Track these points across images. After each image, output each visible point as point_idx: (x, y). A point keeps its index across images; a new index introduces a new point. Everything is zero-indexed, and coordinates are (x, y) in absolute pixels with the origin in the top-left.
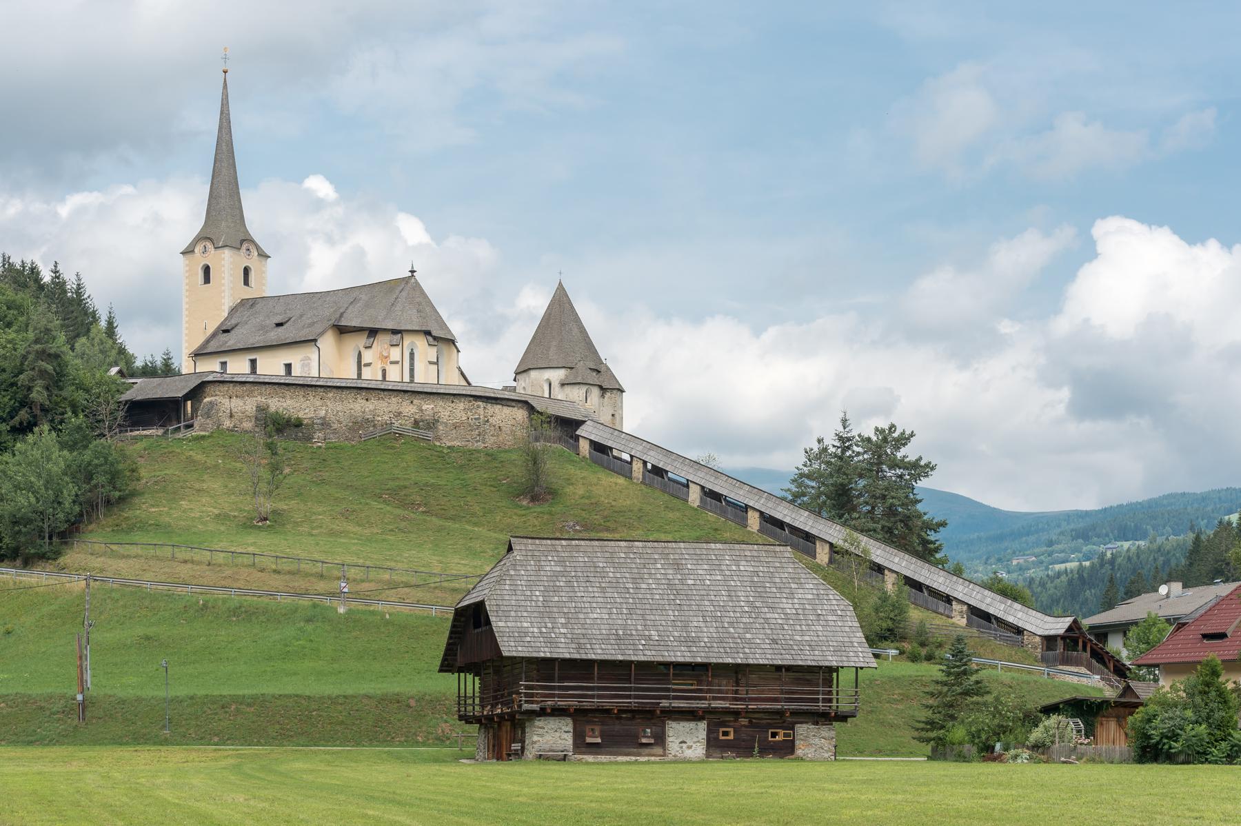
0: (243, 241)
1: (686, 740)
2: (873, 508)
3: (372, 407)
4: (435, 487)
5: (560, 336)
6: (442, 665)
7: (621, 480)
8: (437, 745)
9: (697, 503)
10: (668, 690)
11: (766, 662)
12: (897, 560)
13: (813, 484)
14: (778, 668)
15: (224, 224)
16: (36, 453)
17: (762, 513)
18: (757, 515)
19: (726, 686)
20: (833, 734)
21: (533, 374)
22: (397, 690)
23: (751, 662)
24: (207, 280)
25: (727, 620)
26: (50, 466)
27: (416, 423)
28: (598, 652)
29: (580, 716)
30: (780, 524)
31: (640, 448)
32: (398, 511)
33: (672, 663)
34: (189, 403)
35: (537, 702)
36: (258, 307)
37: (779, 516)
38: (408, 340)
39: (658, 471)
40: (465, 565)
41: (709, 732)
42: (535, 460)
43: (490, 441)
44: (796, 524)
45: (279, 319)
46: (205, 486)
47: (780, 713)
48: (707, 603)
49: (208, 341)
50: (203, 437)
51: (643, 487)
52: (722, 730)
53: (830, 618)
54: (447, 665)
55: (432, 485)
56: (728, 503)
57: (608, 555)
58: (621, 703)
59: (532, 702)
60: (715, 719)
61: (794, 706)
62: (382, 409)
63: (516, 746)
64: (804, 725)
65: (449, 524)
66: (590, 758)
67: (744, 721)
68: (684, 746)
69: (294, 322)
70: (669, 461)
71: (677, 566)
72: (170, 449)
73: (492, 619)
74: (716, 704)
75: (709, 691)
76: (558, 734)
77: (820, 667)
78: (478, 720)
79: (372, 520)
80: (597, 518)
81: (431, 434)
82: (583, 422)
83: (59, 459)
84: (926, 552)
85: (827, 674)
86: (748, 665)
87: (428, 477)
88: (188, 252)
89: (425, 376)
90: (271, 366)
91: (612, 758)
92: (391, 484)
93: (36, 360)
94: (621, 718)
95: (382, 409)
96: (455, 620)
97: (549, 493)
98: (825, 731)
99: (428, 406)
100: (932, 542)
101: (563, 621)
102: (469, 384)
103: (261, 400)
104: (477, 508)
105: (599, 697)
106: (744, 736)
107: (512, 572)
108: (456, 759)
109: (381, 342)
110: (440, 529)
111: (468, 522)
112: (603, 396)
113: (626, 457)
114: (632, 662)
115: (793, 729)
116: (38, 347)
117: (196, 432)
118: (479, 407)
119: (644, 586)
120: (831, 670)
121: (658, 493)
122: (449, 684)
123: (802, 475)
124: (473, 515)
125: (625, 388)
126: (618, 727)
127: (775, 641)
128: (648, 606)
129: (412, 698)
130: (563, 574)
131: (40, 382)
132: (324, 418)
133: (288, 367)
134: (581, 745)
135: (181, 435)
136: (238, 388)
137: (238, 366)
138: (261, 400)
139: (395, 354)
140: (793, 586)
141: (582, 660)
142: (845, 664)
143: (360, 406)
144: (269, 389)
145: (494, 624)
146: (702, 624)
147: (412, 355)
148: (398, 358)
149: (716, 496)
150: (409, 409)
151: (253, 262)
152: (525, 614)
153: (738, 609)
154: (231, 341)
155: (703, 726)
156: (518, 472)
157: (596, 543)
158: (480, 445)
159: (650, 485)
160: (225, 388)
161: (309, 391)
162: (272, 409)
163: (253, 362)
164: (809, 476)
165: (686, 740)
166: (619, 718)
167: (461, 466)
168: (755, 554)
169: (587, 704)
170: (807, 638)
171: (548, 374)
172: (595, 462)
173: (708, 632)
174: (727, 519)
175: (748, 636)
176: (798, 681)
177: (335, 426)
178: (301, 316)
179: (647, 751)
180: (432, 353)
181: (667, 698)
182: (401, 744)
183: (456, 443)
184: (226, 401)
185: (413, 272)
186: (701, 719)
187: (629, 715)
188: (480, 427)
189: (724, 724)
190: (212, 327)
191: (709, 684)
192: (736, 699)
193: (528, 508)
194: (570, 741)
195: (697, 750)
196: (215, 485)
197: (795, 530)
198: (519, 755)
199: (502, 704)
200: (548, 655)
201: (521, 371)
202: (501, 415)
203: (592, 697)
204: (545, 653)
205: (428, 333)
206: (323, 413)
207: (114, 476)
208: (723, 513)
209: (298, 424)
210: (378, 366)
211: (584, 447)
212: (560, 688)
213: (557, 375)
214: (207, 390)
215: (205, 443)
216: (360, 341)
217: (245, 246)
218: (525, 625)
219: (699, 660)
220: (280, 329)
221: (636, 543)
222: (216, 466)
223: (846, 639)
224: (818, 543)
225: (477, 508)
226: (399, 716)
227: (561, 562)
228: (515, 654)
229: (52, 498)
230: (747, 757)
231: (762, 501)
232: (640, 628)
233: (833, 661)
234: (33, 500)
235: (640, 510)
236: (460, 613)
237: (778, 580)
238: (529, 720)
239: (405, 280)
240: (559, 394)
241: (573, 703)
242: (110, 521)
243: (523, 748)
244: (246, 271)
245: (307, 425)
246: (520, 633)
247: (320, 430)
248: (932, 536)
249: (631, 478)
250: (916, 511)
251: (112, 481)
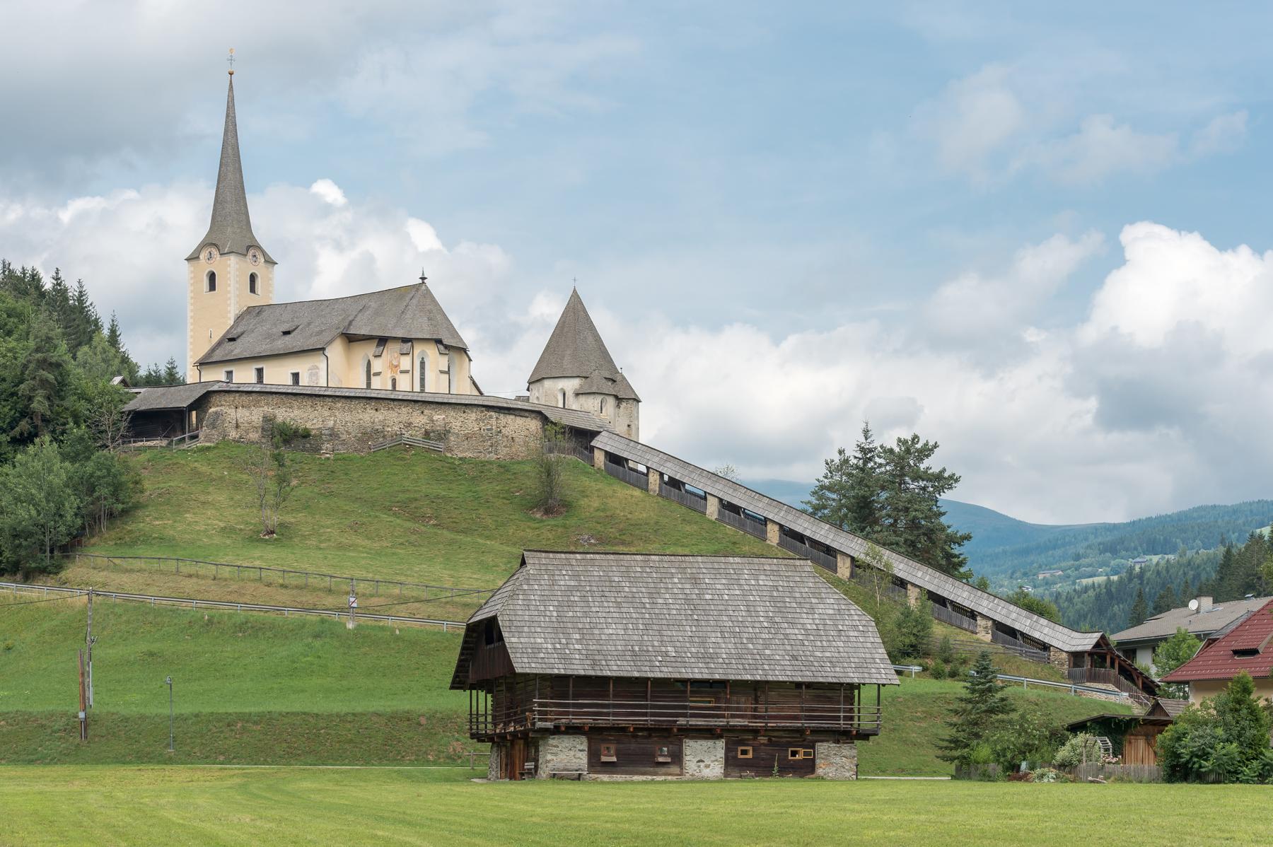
0: (250, 247)
1: (704, 759)
2: (896, 521)
3: (381, 418)
4: (447, 500)
5: (574, 344)
6: (453, 682)
7: (637, 493)
8: (448, 764)
9: (715, 516)
10: (685, 707)
11: (786, 679)
12: (920, 574)
13: (834, 496)
14: (798, 685)
15: (230, 230)
16: (37, 465)
17: (781, 526)
18: (776, 528)
19: (745, 703)
20: (854, 752)
21: (547, 383)
22: (407, 707)
23: (770, 678)
24: (212, 287)
25: (746, 635)
26: (51, 478)
27: (427, 433)
28: (614, 668)
29: (595, 734)
30: (800, 538)
31: (657, 459)
32: (409, 524)
33: (689, 680)
34: (194, 413)
35: (551, 720)
36: (265, 314)
37: (799, 529)
38: (418, 349)
39: (675, 483)
40: (477, 579)
41: (728, 750)
42: (548, 472)
43: (503, 452)
44: (817, 538)
45: (286, 327)
46: (210, 498)
47: (800, 731)
48: (725, 618)
49: (213, 350)
50: (208, 448)
51: (660, 499)
52: (740, 748)
53: (852, 634)
54: (459, 682)
55: (444, 497)
56: (747, 516)
57: (623, 569)
58: (637, 721)
59: (546, 720)
60: (734, 738)
61: (814, 724)
62: (392, 420)
63: (529, 765)
64: (825, 744)
65: (460, 537)
66: (605, 778)
67: (763, 740)
68: (702, 765)
69: (301, 330)
70: (686, 473)
71: (695, 581)
72: (175, 461)
73: (505, 635)
74: (735, 722)
75: (727, 709)
76: (572, 753)
77: (842, 684)
78: (490, 738)
79: (382, 533)
80: (612, 532)
81: (442, 445)
82: (598, 433)
83: (61, 471)
84: (950, 566)
85: (848, 691)
86: (767, 682)
87: (439, 490)
88: (193, 258)
89: (436, 385)
90: (278, 375)
91: (628, 777)
92: (401, 497)
93: (37, 369)
94: (637, 736)
95: (392, 420)
96: (466, 636)
97: (564, 506)
98: (846, 750)
99: (439, 416)
100: (956, 556)
101: (577, 636)
102: (481, 394)
103: (268, 410)
104: (489, 521)
105: (615, 714)
106: (763, 755)
107: (525, 587)
108: (468, 778)
109: (391, 351)
110: (451, 543)
111: (480, 535)
112: (618, 406)
113: (642, 469)
114: (648, 679)
115: (813, 748)
116: (39, 355)
117: (201, 443)
118: (491, 417)
119: (660, 601)
120: (852, 687)
121: (675, 506)
122: (461, 701)
123: (822, 487)
124: (486, 528)
125: (641, 398)
126: (634, 746)
127: (794, 658)
128: (664, 622)
129: (423, 715)
130: (577, 588)
131: (41, 392)
132: (332, 429)
133: (296, 376)
134: (596, 764)
135: (185, 446)
136: (244, 398)
137: (244, 376)
138: (268, 410)
139: (405, 363)
140: (814, 601)
141: (597, 677)
142: (867, 681)
143: (369, 417)
144: (276, 399)
145: (506, 640)
146: (720, 640)
147: (422, 364)
148: (408, 367)
149: (735, 509)
150: (420, 419)
151: (260, 269)
152: (539, 630)
153: (757, 625)
154: (237, 349)
155: (721, 744)
156: (532, 484)
157: (612, 557)
158: (493, 457)
159: (667, 498)
160: (230, 398)
161: (317, 401)
162: (280, 420)
163: (260, 371)
164: (829, 489)
165: (704, 759)
166: (635, 736)
167: (473, 478)
168: (775, 568)
169: (602, 722)
170: (828, 654)
171: (562, 384)
172: (611, 474)
173: (726, 649)
174: (746, 532)
175: (767, 652)
176: (818, 699)
177: (344, 437)
178: (309, 324)
179: (664, 770)
180: (443, 362)
181: (685, 715)
182: (412, 763)
183: (468, 455)
184: (232, 411)
185: (423, 279)
186: (719, 737)
187: (645, 733)
188: (492, 438)
189: (742, 742)
190: (218, 335)
191: (728, 701)
192: (755, 717)
193: (542, 521)
194: (585, 760)
195: (715, 769)
196: (221, 497)
197: (815, 544)
198: (533, 774)
199: (515, 722)
200: (563, 672)
201: (534, 381)
202: (514, 425)
203: (608, 714)
204: (559, 669)
205: (439, 341)
206: (331, 424)
207: (117, 488)
208: (742, 526)
209: (306, 435)
210: (388, 376)
211: (599, 458)
212: (575, 705)
213: (571, 385)
214: (213, 400)
215: (210, 455)
216: (370, 349)
217: (251, 252)
218: (539, 640)
219: (717, 677)
220: (288, 337)
221: (653, 557)
222: (222, 478)
223: (868, 656)
224: (839, 557)
225: (489, 521)
226: (410, 735)
227: (576, 576)
228: (528, 671)
229: (53, 510)
230: (767, 776)
231: (782, 514)
232: (656, 644)
233: (854, 678)
234: (34, 512)
235: (657, 523)
236: (472, 629)
237: (798, 595)
238: (542, 739)
239: (416, 288)
240: (573, 404)
241: (588, 721)
242: (113, 534)
243: (536, 767)
244: (253, 278)
245: (315, 436)
246: (533, 649)
247: (328, 441)
248: (956, 550)
249: (647, 490)
250: (940, 524)
251: (115, 494)
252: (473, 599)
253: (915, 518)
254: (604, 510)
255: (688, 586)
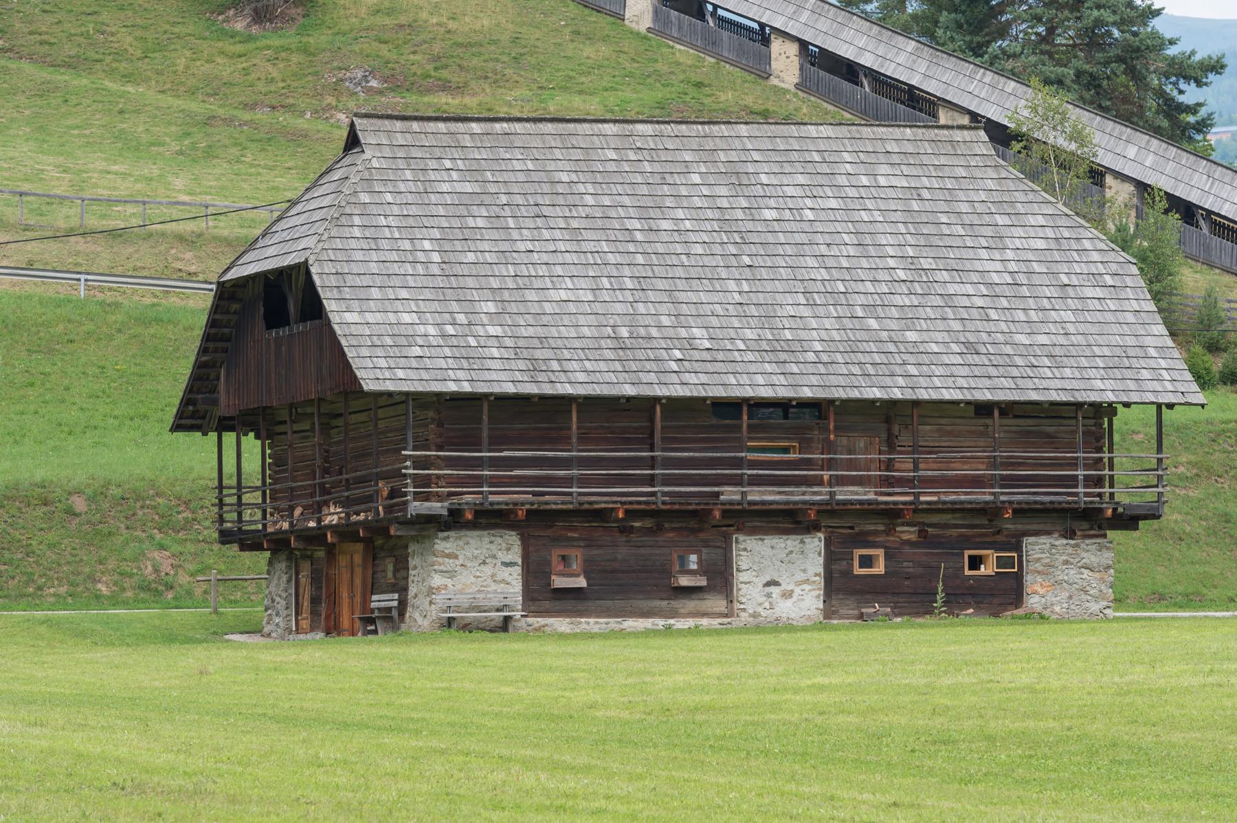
1: (781, 576)
2: (1051, 31)
6: (180, 415)
8: (144, 604)
9: (646, 22)
10: (738, 463)
11: (956, 395)
12: (1132, 151)
14: (983, 409)
17: (803, 45)
18: (793, 49)
19: (866, 451)
20: (1107, 557)
22: (39, 475)
23: (924, 395)
25: (861, 299)
28: (577, 379)
29: (537, 527)
30: (849, 71)
33: (746, 400)
35: (439, 497)
40: (124, 175)
41: (831, 559)
44: (889, 70)
47: (990, 512)
48: (811, 262)
52: (858, 552)
53: (1089, 292)
54: (191, 417)
57: (578, 154)
58: (633, 495)
59: (427, 497)
60: (842, 529)
61: (1020, 496)
63: (381, 600)
64: (1043, 539)
65: (63, 77)
66: (561, 624)
68: (775, 590)
71: (737, 179)
73: (330, 306)
74: (846, 494)
75: (830, 465)
76: (488, 570)
77: (1079, 405)
78: (278, 545)
80: (418, 61)
84: (1180, 128)
85: (1093, 420)
86: (916, 403)
91: (613, 623)
94: (631, 530)
96: (216, 308)
98: (1090, 552)
100: (1193, 109)
101: (491, 307)
104: (127, 40)
105: (584, 481)
107: (365, 198)
108: (216, 634)
110: (44, 91)
111: (111, 73)
114: (656, 400)
115: (1018, 548)
119: (665, 225)
120: (1101, 412)
122: (197, 454)
124: (119, 55)
126: (623, 552)
127: (971, 348)
128: (680, 272)
129: (79, 492)
130: (479, 200)
134: (542, 595)
140: (1001, 220)
141: (543, 398)
142: (1134, 397)
145: (334, 318)
146: (805, 311)
152: (404, 294)
153: (882, 275)
155: (815, 544)
157: (549, 127)
165: (781, 576)
166: (625, 530)
168: (910, 148)
169: (553, 499)
170: (1043, 339)
173: (820, 329)
174: (720, 58)
175: (911, 336)
176: (1026, 438)
179: (691, 604)
182: (60, 602)
186: (811, 528)
187: (649, 523)
189: (863, 540)
192: (888, 482)
193: (249, 39)
195: (807, 600)
197: (883, 84)
198: (394, 619)
199: (346, 503)
200: (467, 388)
203: (568, 481)
204: (458, 383)
208: (710, 45)
212: (495, 463)
218: (407, 318)
219: (807, 393)
221: (641, 128)
223: (1130, 341)
225: (127, 40)
226: (51, 537)
227: (472, 173)
228: (390, 386)
230: (918, 614)
231: (805, 16)
232: (665, 321)
233: (1102, 390)
235: (515, 40)
236: (230, 296)
237: (964, 208)
238: (416, 539)
241: (522, 497)
243: (403, 605)
246: (400, 332)
248: (1190, 94)
250: (1155, 35)
252: (225, 228)
253: (1099, 23)
254: (390, 12)
255: (723, 191)
